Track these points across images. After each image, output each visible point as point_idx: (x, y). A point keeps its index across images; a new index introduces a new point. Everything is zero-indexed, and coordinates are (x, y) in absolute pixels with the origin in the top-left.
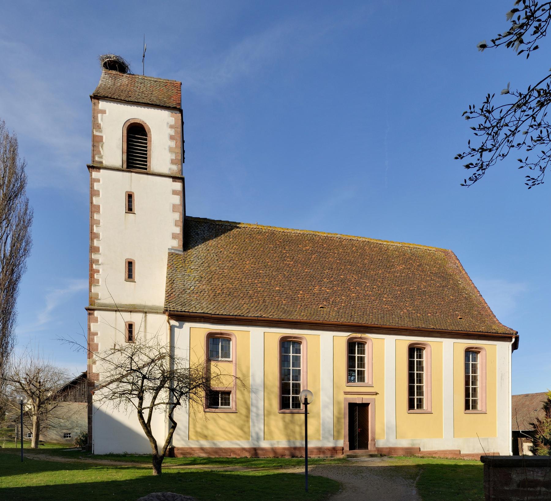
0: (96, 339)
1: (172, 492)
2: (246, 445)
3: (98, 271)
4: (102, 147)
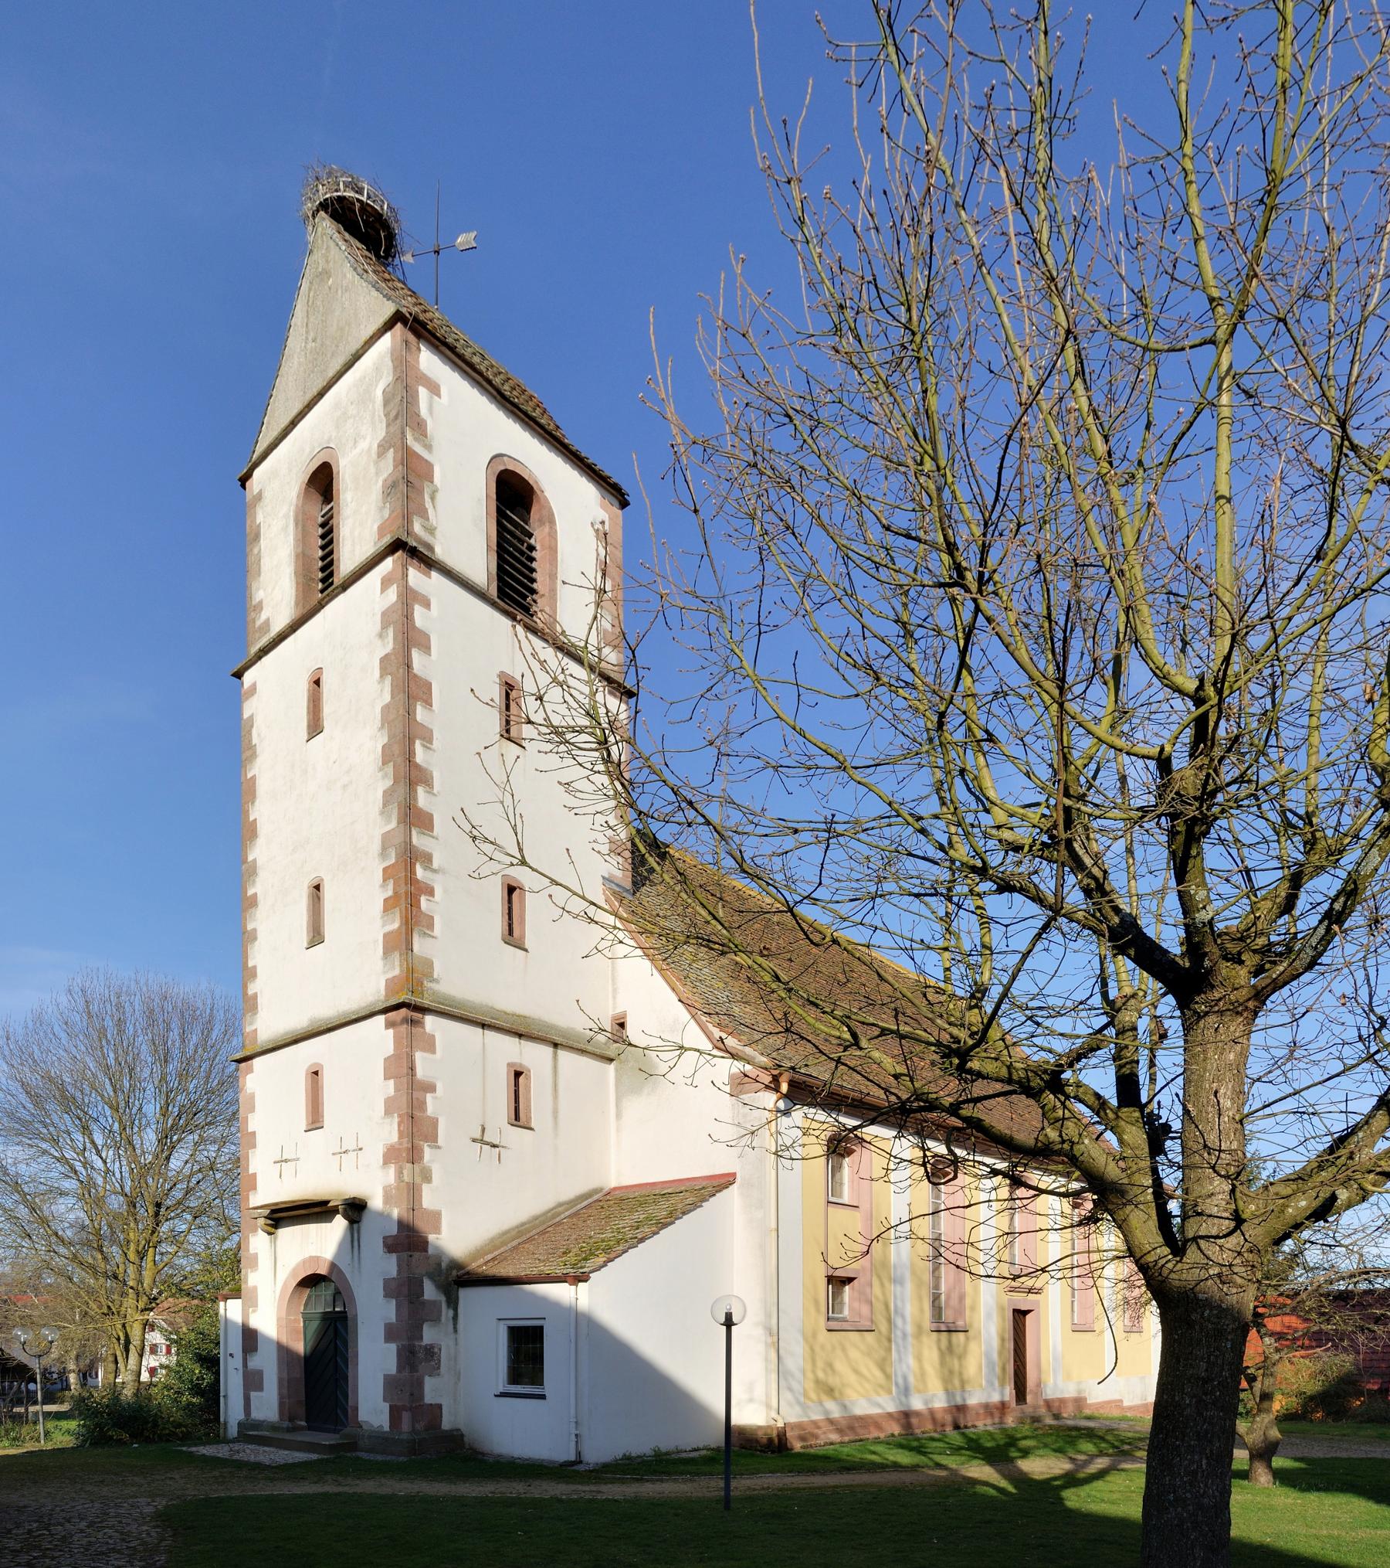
0: (432, 1105)
1: (1271, 1508)
2: (891, 1408)
3: (431, 892)
4: (433, 499)
